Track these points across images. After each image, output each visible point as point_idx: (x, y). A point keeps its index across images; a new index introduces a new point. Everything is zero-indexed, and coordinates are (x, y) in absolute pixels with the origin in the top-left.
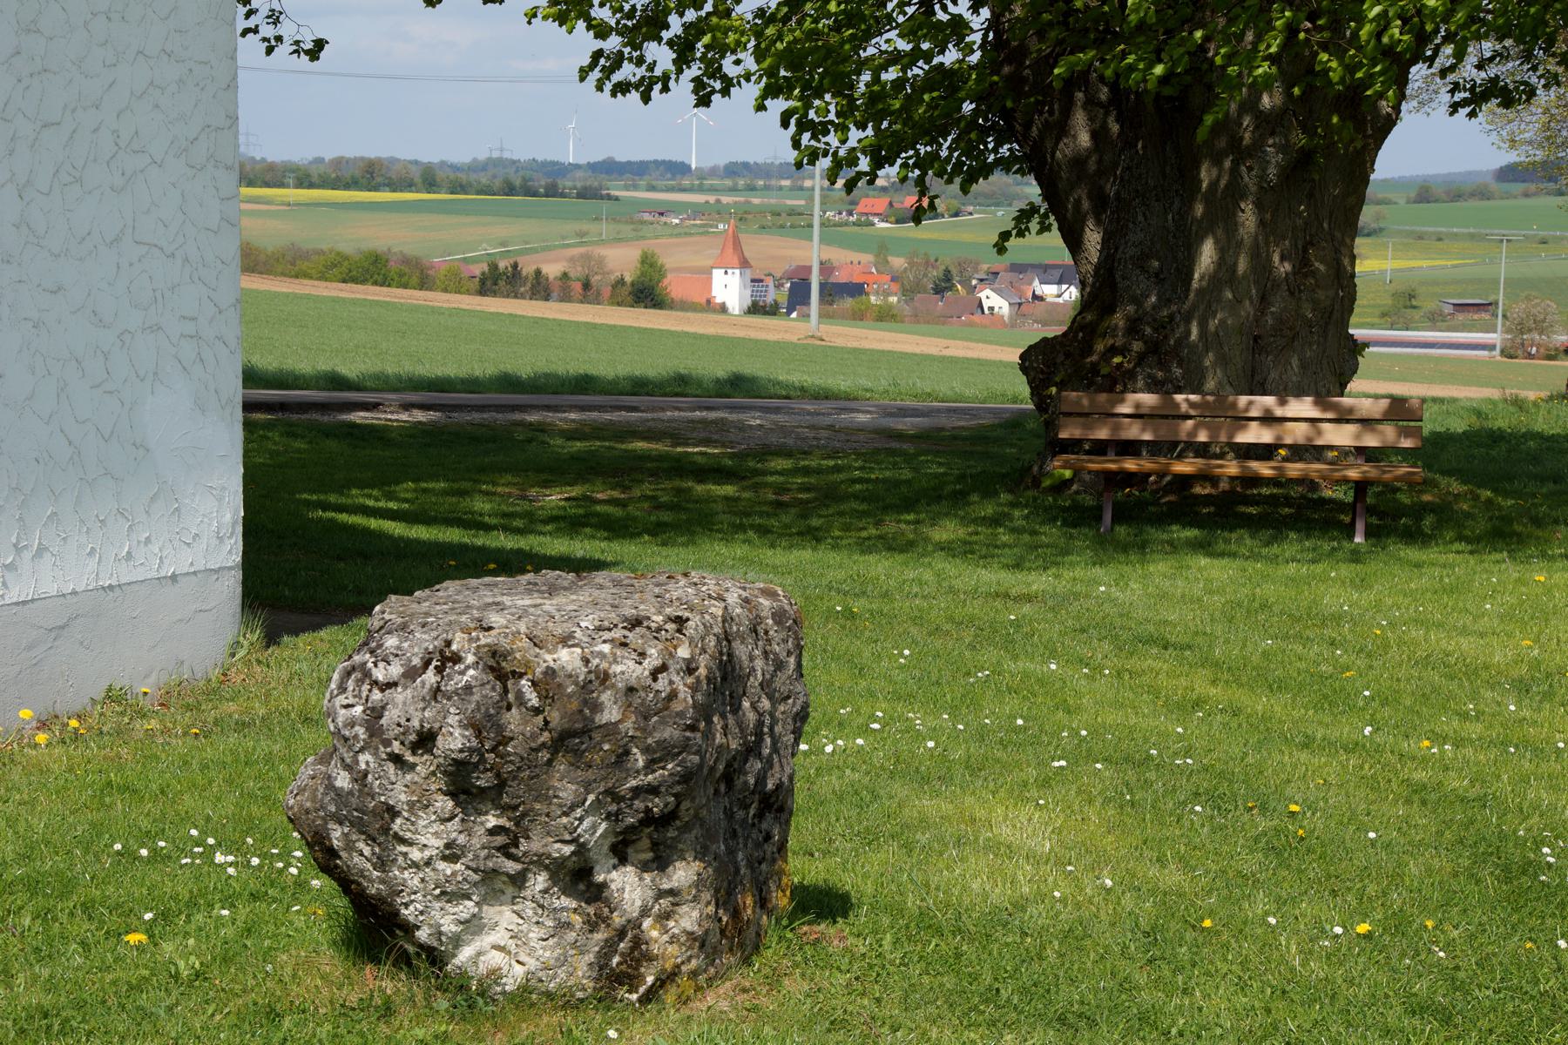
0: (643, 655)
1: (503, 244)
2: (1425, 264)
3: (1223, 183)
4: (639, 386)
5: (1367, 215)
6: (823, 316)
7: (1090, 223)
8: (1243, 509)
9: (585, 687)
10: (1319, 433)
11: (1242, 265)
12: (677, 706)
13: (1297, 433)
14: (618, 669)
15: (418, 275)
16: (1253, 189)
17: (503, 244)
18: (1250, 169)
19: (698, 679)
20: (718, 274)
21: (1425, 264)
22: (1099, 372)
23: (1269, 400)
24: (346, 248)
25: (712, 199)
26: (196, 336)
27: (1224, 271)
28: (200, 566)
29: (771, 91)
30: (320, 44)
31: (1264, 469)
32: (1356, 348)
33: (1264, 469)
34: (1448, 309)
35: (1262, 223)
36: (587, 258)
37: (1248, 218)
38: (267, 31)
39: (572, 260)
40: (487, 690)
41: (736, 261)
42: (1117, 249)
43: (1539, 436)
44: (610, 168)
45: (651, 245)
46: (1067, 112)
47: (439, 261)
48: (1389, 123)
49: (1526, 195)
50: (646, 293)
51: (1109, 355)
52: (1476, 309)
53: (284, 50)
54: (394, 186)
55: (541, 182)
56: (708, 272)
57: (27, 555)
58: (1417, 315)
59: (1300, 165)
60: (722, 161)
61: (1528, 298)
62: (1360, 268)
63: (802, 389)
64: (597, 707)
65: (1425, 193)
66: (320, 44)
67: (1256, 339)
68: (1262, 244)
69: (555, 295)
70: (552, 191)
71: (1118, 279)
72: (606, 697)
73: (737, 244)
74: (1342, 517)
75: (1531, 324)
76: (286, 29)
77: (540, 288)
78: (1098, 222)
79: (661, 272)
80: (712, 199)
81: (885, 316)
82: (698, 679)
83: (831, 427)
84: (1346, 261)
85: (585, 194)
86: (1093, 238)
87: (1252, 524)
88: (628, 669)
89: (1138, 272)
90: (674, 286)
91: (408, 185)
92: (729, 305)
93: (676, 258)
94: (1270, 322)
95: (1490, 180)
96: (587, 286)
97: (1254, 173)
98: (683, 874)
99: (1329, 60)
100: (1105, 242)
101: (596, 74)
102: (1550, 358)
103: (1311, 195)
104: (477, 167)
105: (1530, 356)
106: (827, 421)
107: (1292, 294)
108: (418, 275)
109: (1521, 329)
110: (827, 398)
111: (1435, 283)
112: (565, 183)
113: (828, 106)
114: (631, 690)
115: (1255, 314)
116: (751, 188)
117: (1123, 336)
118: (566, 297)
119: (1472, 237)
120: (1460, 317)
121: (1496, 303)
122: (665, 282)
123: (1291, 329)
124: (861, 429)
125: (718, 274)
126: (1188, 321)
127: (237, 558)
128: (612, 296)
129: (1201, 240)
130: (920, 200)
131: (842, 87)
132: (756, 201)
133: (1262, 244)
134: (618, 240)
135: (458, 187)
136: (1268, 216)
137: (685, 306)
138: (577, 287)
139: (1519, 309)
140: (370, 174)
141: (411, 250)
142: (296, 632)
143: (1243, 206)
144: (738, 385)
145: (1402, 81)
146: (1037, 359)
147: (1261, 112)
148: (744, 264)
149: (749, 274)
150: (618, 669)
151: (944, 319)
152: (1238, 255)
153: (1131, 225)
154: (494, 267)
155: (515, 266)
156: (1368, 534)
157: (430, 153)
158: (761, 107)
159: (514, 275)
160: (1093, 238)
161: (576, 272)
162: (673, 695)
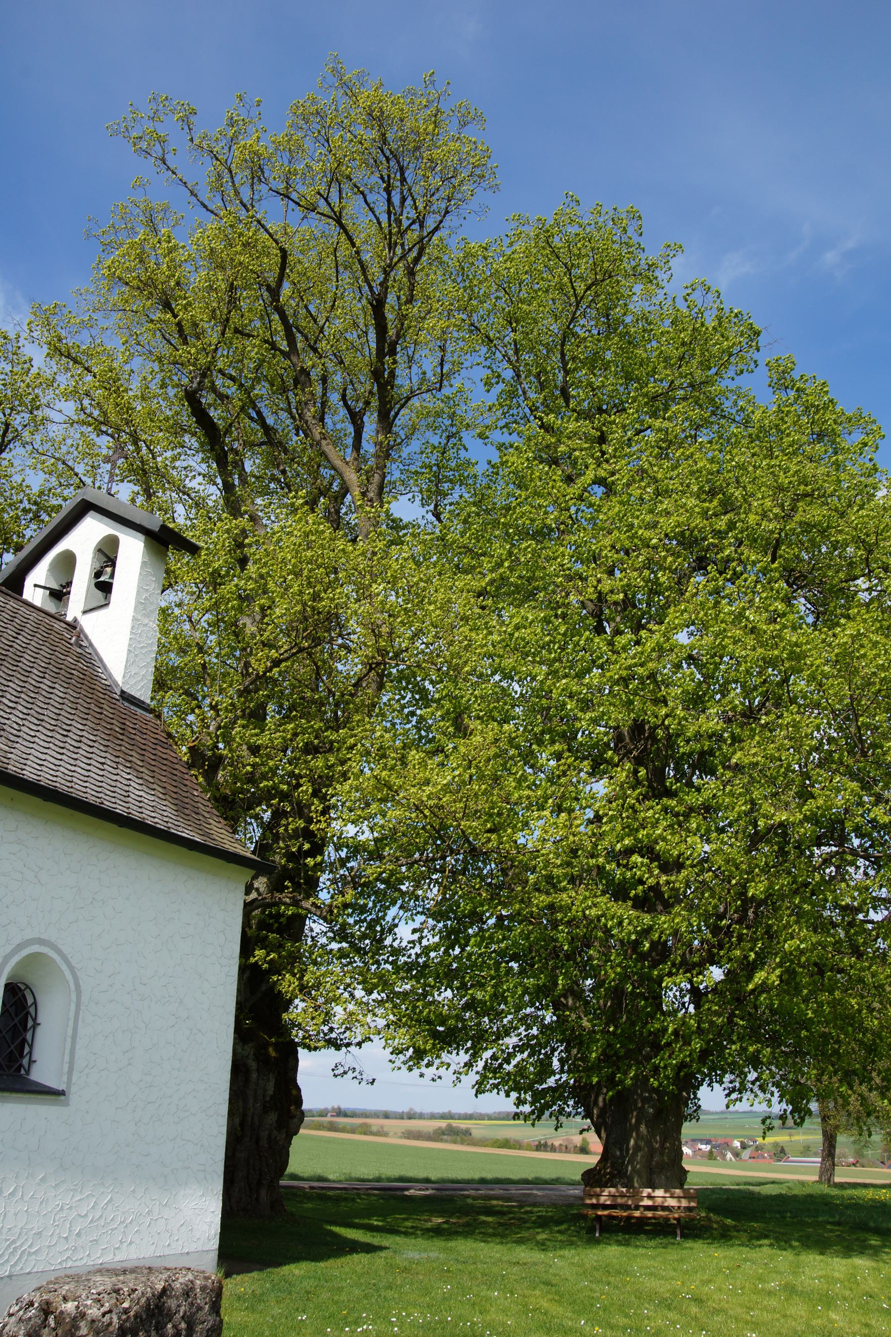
0: (102, 1306)
9: (74, 1319)
12: (111, 1329)
13: (659, 1201)
14: (90, 1311)
15: (517, 1145)
19: (128, 1317)
23: (650, 1190)
24: (499, 1137)
26: (204, 1171)
27: (637, 1148)
28: (200, 1249)
31: (649, 1214)
32: (685, 1172)
33: (649, 1214)
40: (37, 1320)
53: (364, 1083)
57: (125, 1244)
64: (78, 1328)
72: (82, 1324)
77: (553, 1149)
79: (588, 1143)
82: (128, 1317)
87: (647, 1233)
88: (94, 1312)
108: (517, 1145)
114: (93, 1321)
118: (561, 1151)
127: (217, 1246)
142: (238, 1273)
150: (90, 1311)
157: (399, 1109)
159: (545, 1145)
160: (603, 1135)
162: (110, 1324)
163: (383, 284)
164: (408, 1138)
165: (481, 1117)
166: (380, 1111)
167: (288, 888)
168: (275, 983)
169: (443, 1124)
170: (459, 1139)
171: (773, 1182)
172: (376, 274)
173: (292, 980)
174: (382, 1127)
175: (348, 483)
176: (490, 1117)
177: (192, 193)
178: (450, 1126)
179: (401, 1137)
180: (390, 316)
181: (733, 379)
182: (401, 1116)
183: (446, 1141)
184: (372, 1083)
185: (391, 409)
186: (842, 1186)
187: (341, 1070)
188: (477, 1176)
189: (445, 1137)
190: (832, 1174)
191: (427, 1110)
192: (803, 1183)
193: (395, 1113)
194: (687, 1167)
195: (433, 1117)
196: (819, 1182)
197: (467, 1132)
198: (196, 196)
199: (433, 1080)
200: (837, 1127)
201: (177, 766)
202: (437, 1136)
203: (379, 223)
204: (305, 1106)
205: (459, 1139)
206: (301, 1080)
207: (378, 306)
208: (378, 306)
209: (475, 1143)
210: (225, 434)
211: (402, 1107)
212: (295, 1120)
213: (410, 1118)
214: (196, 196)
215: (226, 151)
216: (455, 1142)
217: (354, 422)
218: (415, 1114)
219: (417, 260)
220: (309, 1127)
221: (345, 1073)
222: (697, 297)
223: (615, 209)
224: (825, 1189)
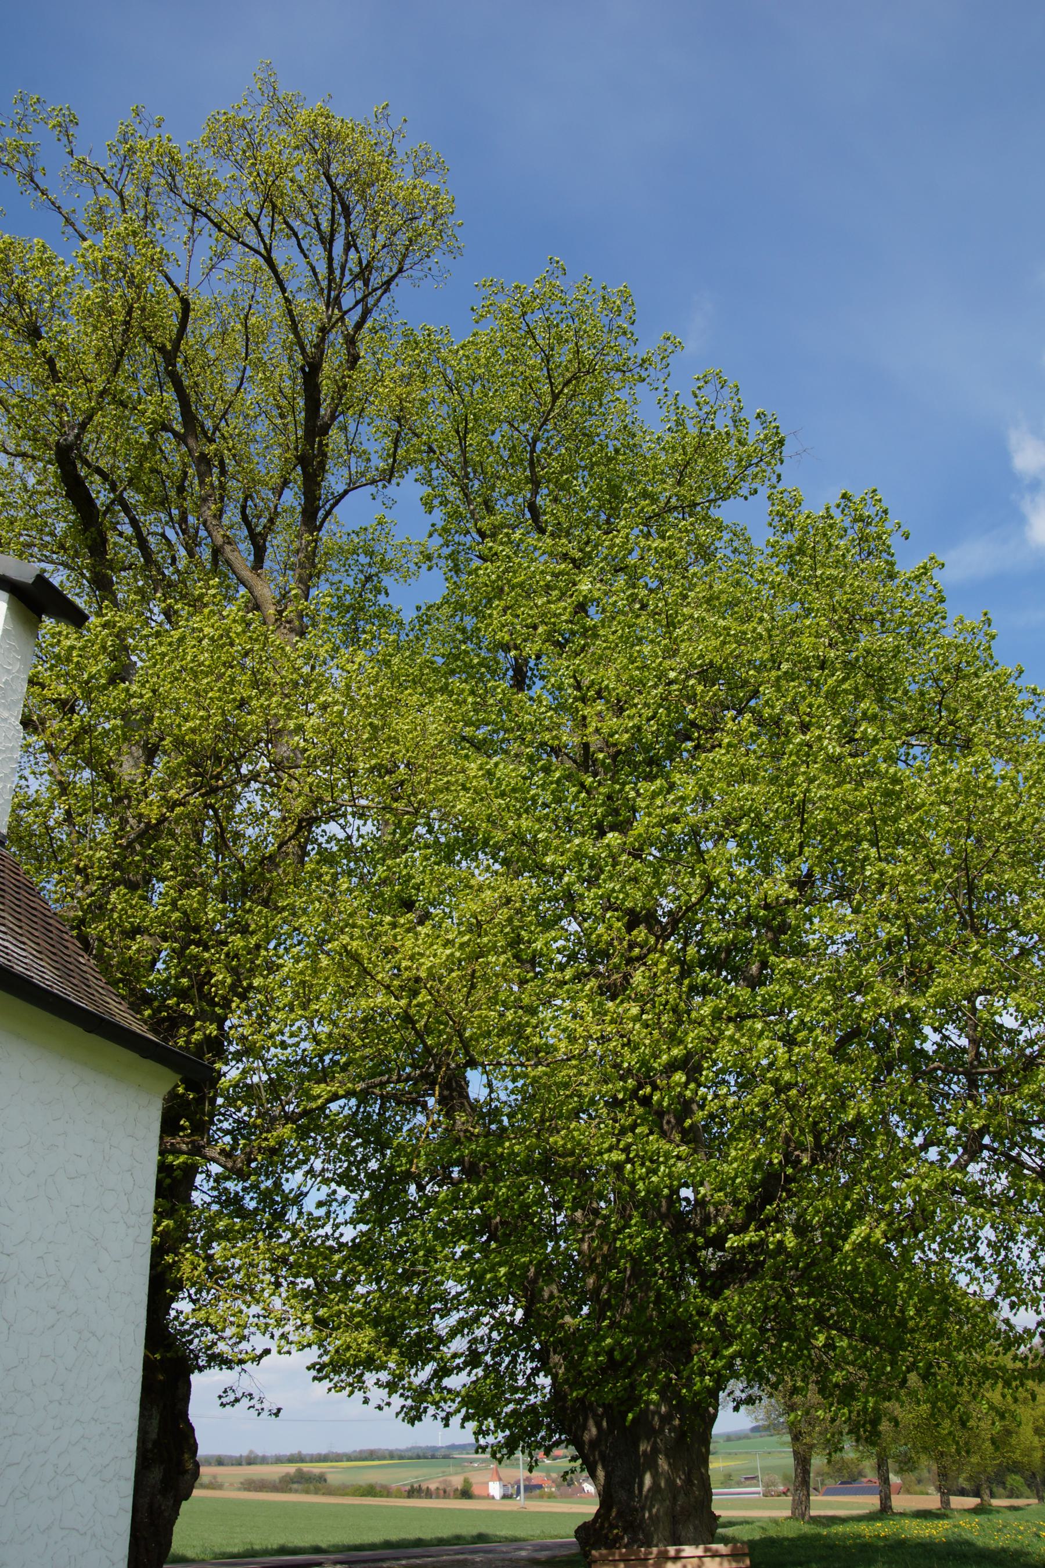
4: (441, 1542)
5: (712, 1447)
6: (526, 1498)
15: (385, 1492)
20: (491, 1484)
27: (655, 1486)
29: (466, 1418)
30: (279, 1410)
37: (663, 1464)
38: (258, 1406)
43: (787, 1539)
44: (453, 1447)
45: (468, 1475)
46: (586, 1420)
47: (394, 1486)
48: (715, 1416)
50: (466, 1493)
52: (752, 1479)
53: (265, 1413)
54: (379, 1459)
55: (429, 1454)
59: (682, 1435)
60: (449, 1443)
62: (711, 1466)
65: (729, 1438)
66: (279, 1410)
70: (433, 1457)
76: (265, 1405)
77: (428, 1494)
81: (551, 1496)
83: (510, 1560)
85: (445, 1457)
90: (476, 1490)
91: (384, 1458)
93: (476, 1478)
98: (72, 517)
101: (402, 1415)
104: (408, 1450)
106: (509, 1556)
108: (385, 1492)
112: (438, 1454)
113: (490, 1423)
118: (438, 1497)
124: (522, 1559)
125: (491, 1484)
129: (644, 1473)
131: (496, 1416)
134: (456, 1474)
135: (401, 1458)
137: (479, 1497)
140: (371, 1455)
141: (384, 1482)
144: (481, 1538)
145: (717, 1399)
148: (500, 1479)
151: (571, 1496)
157: (236, 1453)
158: (463, 1427)
160: (601, 1473)
163: (319, 346)
164: (248, 1489)
165: (338, 1458)
166: (212, 1457)
167: (183, 1128)
168: (170, 1266)
169: (291, 1469)
170: (312, 1487)
171: (741, 1523)
172: (310, 334)
173: (196, 1260)
174: (215, 1477)
175: (260, 600)
176: (349, 1458)
177: (67, 220)
178: (299, 1471)
179: (239, 1489)
180: (326, 387)
181: (746, 498)
182: (238, 1462)
183: (296, 1491)
184: (277, 1414)
185: (319, 509)
186: (816, 1520)
187: (231, 1397)
188: (376, 1538)
189: (295, 1486)
190: (807, 1507)
191: (271, 1451)
192: (775, 1521)
193: (230, 1457)
194: (717, 1513)
195: (279, 1460)
196: (793, 1517)
197: (322, 1478)
198: (72, 225)
199: (380, 1408)
200: (811, 1447)
201: (51, 921)
202: (285, 1485)
203: (315, 274)
204: (202, 1452)
205: (312, 1487)
206: (192, 1418)
207: (311, 373)
208: (311, 373)
209: (331, 1492)
210: (105, 513)
211: (240, 1450)
212: (188, 1477)
213: (249, 1464)
214: (72, 225)
215: (116, 171)
216: (307, 1492)
217: (254, 543)
218: (257, 1457)
219: (359, 326)
220: (204, 1486)
221: (237, 1400)
222: (708, 394)
223: (604, 288)
224: (807, 1529)
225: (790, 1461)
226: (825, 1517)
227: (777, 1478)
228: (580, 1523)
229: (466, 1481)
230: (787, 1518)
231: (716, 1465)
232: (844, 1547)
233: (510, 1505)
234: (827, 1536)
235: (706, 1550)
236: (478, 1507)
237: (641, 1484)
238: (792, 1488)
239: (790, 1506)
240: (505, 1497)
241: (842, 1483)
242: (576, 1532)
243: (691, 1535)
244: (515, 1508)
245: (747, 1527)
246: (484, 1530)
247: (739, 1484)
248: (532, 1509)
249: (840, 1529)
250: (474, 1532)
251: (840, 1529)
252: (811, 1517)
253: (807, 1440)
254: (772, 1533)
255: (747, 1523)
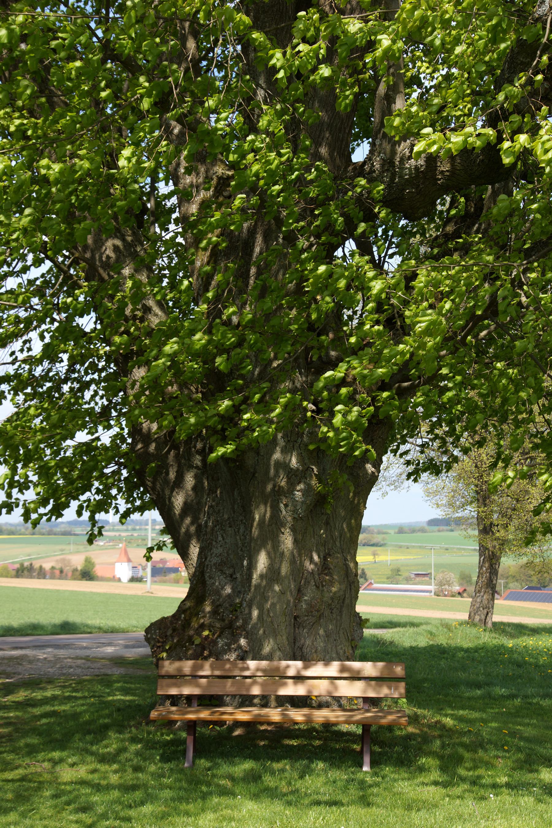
1: (29, 555)
2: (403, 558)
3: (268, 515)
6: (153, 582)
7: (194, 542)
8: (288, 742)
10: (336, 688)
11: (285, 569)
16: (289, 519)
17: (29, 555)
18: (286, 506)
20: (118, 565)
21: (403, 558)
22: (193, 642)
25: (117, 534)
34: (413, 576)
35: (296, 541)
36: (63, 560)
39: (57, 561)
41: (125, 559)
42: (206, 559)
43: (461, 649)
45: (89, 554)
49: (439, 531)
51: (200, 630)
56: (113, 564)
58: (401, 578)
61: (443, 572)
63: (100, 628)
67: (296, 618)
68: (296, 555)
69: (48, 577)
71: (207, 579)
73: (126, 553)
74: (355, 746)
75: (444, 582)
77: (41, 574)
78: (198, 540)
79: (93, 565)
80: (117, 534)
84: (352, 565)
86: (194, 550)
89: (219, 573)
90: (99, 571)
92: (122, 580)
94: (304, 606)
95: (425, 525)
96: (61, 571)
97: (289, 508)
99: (328, 432)
100: (200, 554)
102: (453, 596)
103: (327, 523)
105: (445, 596)
107: (318, 587)
109: (441, 584)
110: (112, 632)
111: (407, 566)
115: (294, 602)
116: (134, 530)
117: (210, 617)
118: (53, 577)
119: (420, 547)
120: (418, 579)
121: (431, 574)
122: (95, 569)
123: (318, 611)
125: (118, 565)
126: (250, 607)
128: (73, 575)
129: (258, 552)
130: (92, 529)
132: (136, 535)
133: (296, 555)
134: (78, 552)
136: (300, 537)
137: (103, 579)
138: (57, 572)
139: (440, 576)
143: (283, 530)
146: (155, 633)
147: (292, 469)
148: (129, 560)
149: (131, 565)
152: (281, 562)
153: (214, 543)
154: (22, 565)
155: (31, 564)
156: (373, 764)
160: (194, 550)
161: (58, 566)
186: (500, 628)
192: (446, 626)
196: (471, 622)
200: (504, 543)
225: (475, 559)
226: (509, 625)
227: (453, 577)
228: (155, 618)
229: (88, 561)
230: (461, 624)
231: (361, 537)
232: (537, 666)
233: (137, 589)
234: (511, 651)
235: (343, 669)
236: (94, 590)
237: (252, 566)
238: (471, 589)
239: (468, 608)
240: (133, 580)
241: (530, 588)
242: (148, 630)
243: (320, 644)
244: (139, 593)
245: (412, 630)
246: (74, 618)
247: (408, 580)
248: (160, 594)
249: (530, 642)
250: (58, 619)
251: (530, 642)
252: (494, 624)
253: (501, 534)
254: (442, 640)
255: (413, 625)
